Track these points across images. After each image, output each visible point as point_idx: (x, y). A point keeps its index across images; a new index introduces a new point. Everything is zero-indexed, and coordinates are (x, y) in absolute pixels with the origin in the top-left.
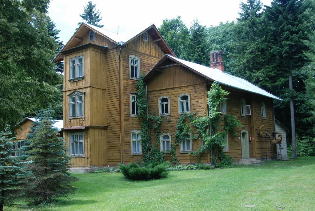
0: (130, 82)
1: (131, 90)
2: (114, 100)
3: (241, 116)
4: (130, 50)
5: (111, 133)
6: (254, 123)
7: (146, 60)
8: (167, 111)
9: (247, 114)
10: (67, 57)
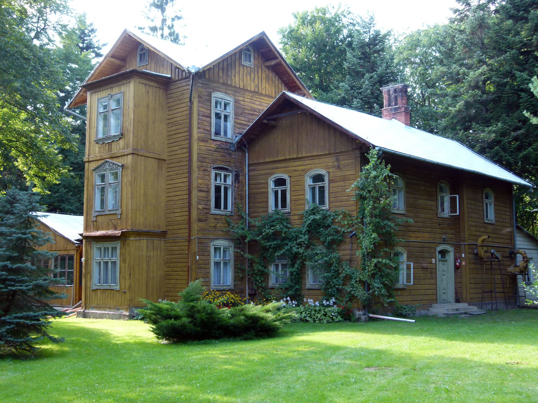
0: (213, 145)
1: (214, 162)
2: (179, 181)
3: (439, 216)
4: (214, 82)
5: (173, 244)
6: (467, 232)
7: (248, 102)
8: (284, 205)
9: (452, 212)
10: (94, 97)
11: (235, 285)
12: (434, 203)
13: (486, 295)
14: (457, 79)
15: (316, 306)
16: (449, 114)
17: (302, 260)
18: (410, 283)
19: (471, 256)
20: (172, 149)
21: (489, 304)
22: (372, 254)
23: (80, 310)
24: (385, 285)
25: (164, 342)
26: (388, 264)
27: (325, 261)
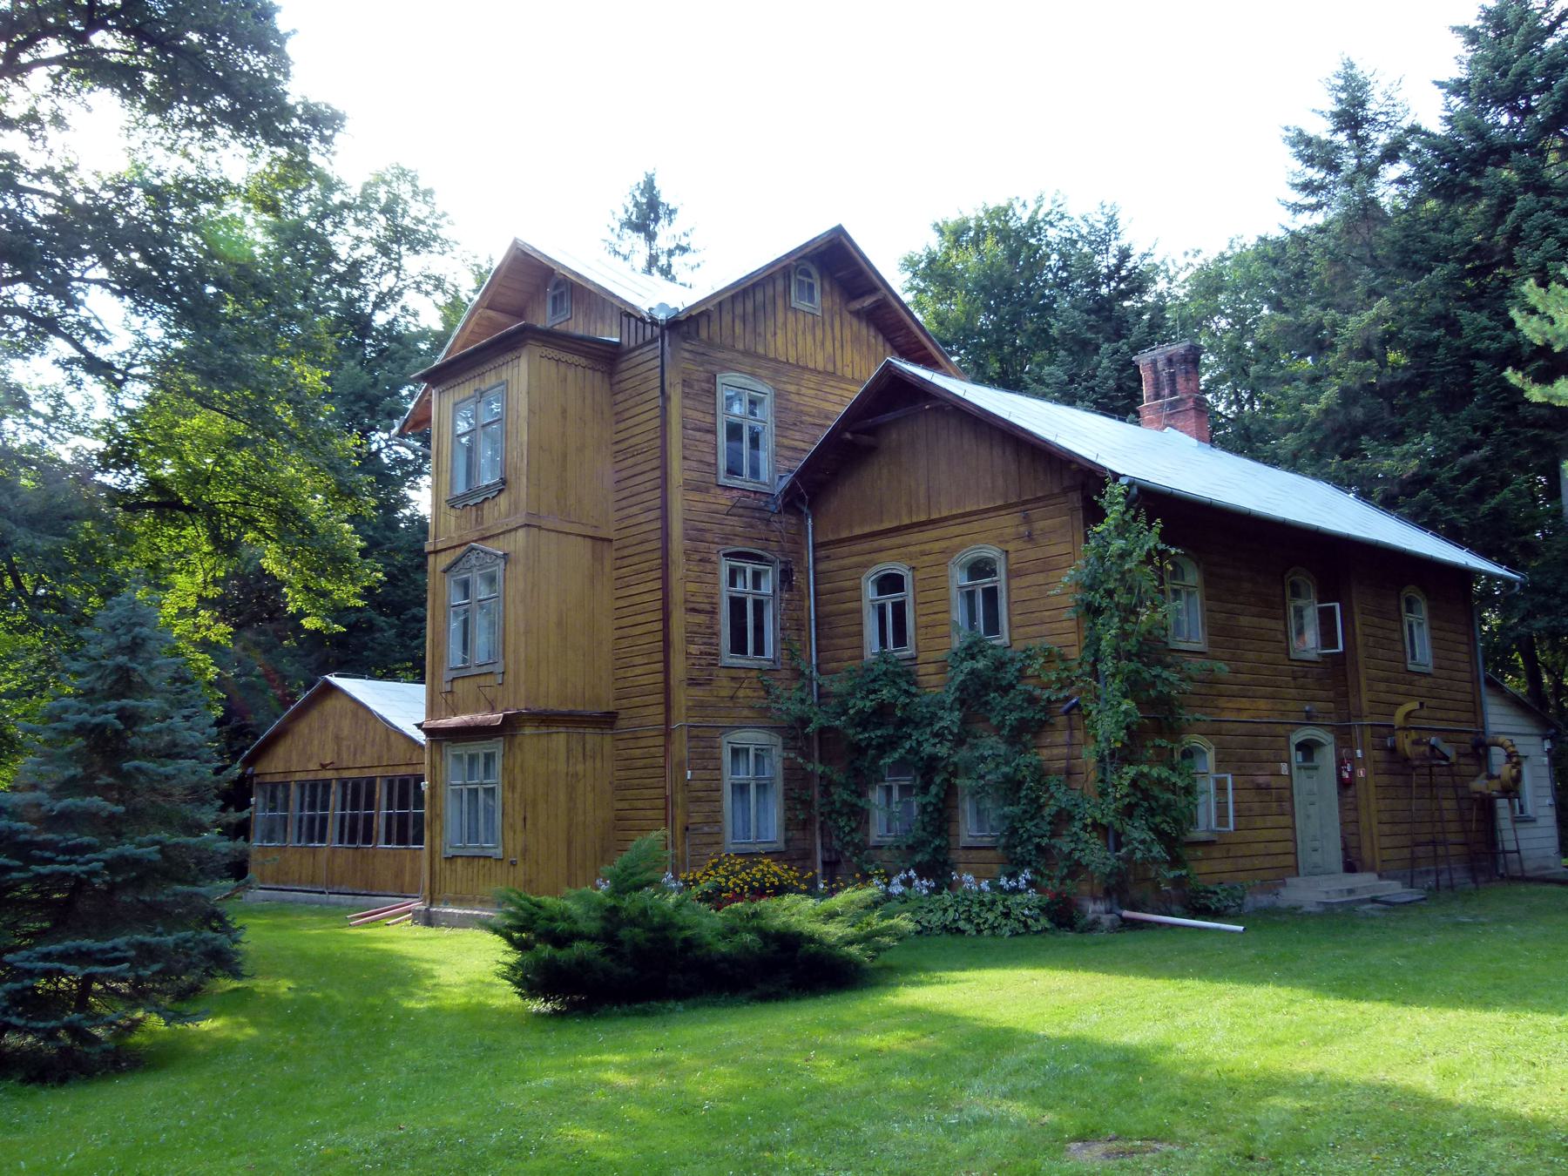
0: (724, 500)
1: (727, 538)
2: (642, 588)
3: (1292, 656)
4: (722, 347)
5: (631, 744)
8: (900, 639)
9: (1324, 646)
11: (787, 841)
12: (1280, 625)
13: (1420, 851)
14: (1319, 346)
15: (981, 891)
16: (1304, 419)
17: (946, 775)
18: (1227, 825)
19: (1378, 755)
20: (626, 512)
21: (1428, 872)
22: (1124, 755)
23: (418, 905)
24: (1161, 835)
25: (538, 1006)
26: (1168, 779)
27: (1005, 775)
